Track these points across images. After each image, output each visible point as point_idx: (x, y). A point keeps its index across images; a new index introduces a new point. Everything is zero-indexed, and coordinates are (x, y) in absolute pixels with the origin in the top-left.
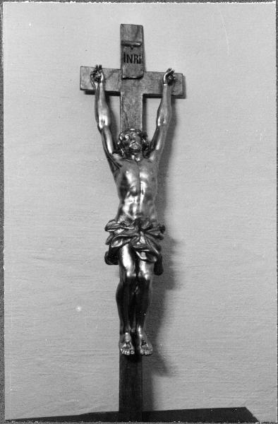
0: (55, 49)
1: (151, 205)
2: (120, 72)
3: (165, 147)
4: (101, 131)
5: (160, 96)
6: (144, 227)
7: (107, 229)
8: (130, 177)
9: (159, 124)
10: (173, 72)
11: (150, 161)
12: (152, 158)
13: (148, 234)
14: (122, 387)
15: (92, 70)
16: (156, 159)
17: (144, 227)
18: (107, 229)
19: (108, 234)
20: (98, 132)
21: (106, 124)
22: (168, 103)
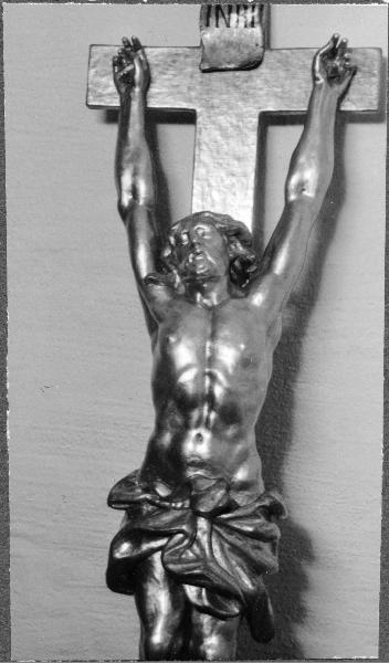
0: (58, 67)
1: (238, 437)
2: (199, 52)
3: (319, 253)
4: (126, 214)
5: (302, 119)
6: (206, 506)
7: (113, 501)
8: (184, 354)
9: (293, 197)
10: (344, 45)
11: (247, 308)
12: (258, 299)
13: (223, 524)
14: (271, 117)
15: (116, 51)
16: (270, 301)
17: (206, 506)
18: (113, 501)
19: (117, 519)
20: (118, 217)
21: (193, 433)
22: (324, 140)
